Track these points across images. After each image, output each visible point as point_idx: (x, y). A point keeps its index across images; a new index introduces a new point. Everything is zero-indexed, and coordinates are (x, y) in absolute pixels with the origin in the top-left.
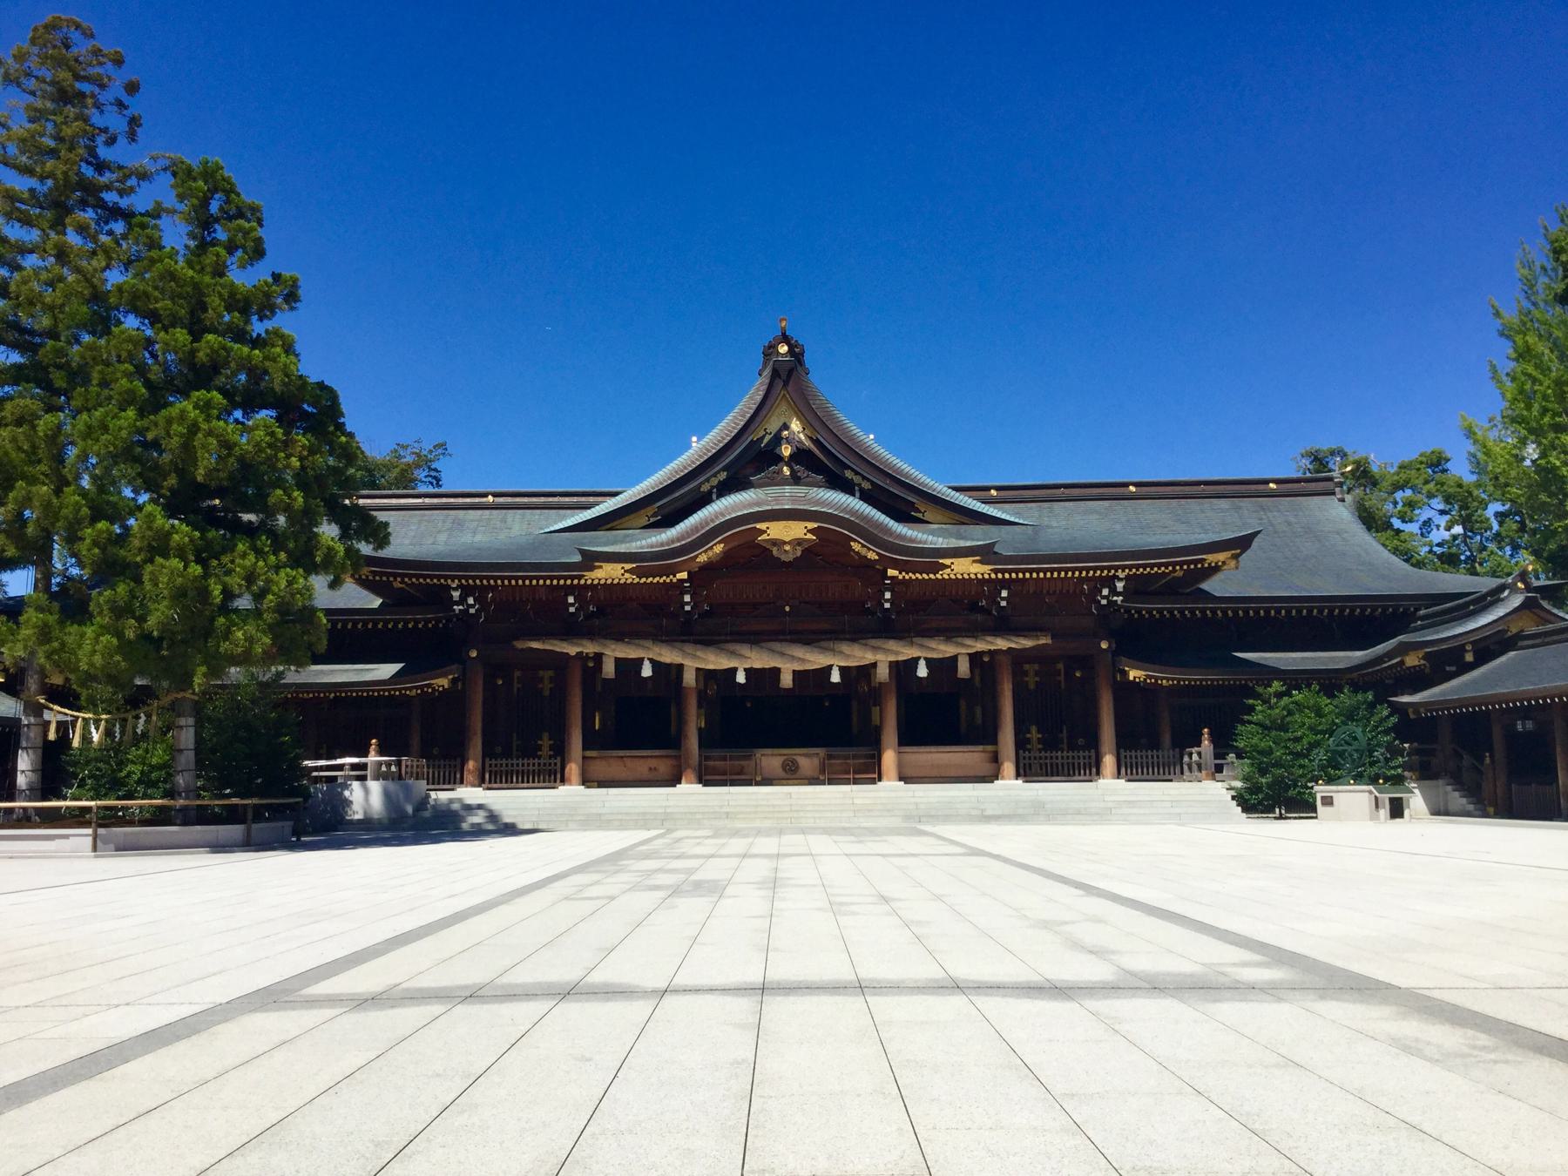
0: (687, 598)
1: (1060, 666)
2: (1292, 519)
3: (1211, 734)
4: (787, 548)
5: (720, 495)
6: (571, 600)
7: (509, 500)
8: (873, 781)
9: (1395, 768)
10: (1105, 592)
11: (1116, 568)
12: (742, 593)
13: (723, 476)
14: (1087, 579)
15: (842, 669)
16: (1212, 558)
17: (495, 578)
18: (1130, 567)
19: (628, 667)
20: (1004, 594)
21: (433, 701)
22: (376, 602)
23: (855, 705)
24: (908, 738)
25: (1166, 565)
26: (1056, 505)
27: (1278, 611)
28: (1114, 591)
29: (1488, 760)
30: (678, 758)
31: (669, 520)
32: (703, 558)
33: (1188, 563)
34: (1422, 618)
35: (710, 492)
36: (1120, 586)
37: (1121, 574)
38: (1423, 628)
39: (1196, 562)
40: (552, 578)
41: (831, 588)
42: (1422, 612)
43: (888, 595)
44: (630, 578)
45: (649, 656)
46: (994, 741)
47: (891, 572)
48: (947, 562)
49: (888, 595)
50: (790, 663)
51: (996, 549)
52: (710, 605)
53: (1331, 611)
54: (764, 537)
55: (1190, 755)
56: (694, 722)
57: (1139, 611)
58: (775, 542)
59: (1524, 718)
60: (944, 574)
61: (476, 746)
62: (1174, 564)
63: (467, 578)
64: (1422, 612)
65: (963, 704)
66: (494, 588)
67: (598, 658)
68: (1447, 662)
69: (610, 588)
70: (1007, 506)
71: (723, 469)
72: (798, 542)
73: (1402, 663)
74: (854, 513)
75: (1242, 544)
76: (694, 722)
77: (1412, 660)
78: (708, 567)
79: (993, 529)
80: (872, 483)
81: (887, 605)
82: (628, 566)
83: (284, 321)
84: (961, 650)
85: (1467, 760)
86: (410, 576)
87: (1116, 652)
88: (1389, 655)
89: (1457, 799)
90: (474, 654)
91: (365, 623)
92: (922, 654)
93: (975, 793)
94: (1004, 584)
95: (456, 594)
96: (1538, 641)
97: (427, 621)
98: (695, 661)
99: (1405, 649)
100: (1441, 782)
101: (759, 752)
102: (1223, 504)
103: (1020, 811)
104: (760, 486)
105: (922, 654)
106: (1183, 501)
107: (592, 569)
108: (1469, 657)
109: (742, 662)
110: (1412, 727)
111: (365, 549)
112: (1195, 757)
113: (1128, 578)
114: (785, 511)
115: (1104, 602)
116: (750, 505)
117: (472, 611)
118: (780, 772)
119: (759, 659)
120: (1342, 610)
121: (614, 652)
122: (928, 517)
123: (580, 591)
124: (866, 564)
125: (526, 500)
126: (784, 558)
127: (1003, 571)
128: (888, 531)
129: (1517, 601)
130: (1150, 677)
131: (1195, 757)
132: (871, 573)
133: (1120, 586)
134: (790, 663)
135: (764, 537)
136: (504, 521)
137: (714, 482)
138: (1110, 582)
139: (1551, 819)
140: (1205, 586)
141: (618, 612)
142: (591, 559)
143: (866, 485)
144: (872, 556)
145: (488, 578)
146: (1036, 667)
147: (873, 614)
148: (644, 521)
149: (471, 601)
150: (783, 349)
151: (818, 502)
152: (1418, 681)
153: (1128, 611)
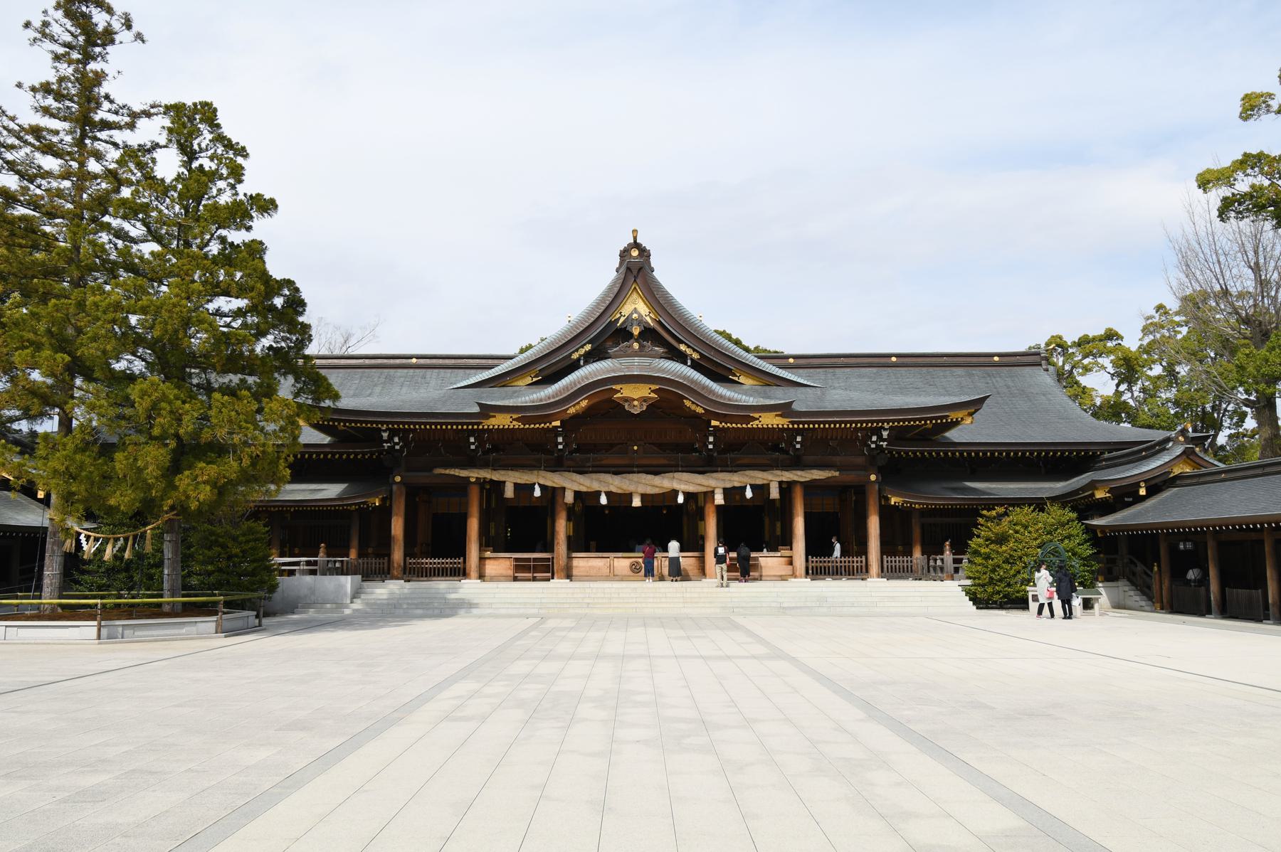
0: (560, 439)
2: (1010, 384)
4: (636, 403)
5: (586, 363)
6: (472, 440)
7: (428, 361)
9: (159, 538)
10: (874, 438)
11: (883, 422)
12: (600, 431)
13: (588, 347)
15: (725, 490)
16: (954, 415)
17: (415, 424)
18: (893, 421)
19: (527, 489)
20: (799, 439)
21: (365, 513)
22: (326, 439)
23: (685, 519)
24: (491, 542)
25: (920, 420)
26: (837, 370)
27: (1000, 453)
28: (880, 438)
29: (1156, 568)
31: (550, 378)
32: (572, 411)
33: (936, 418)
34: (1106, 460)
35: (579, 360)
36: (885, 434)
38: (1108, 467)
39: (941, 418)
40: (457, 424)
41: (674, 431)
42: (1106, 455)
43: (711, 439)
44: (517, 425)
45: (540, 480)
46: (702, 549)
47: (714, 423)
48: (756, 415)
49: (711, 439)
52: (578, 445)
53: (1039, 454)
54: (619, 395)
55: (935, 560)
56: (562, 527)
57: (899, 452)
58: (626, 400)
59: (1185, 541)
60: (755, 424)
61: (355, 542)
62: (926, 419)
63: (393, 423)
64: (1106, 455)
67: (501, 484)
68: (1125, 496)
69: (502, 431)
70: (801, 371)
71: (588, 342)
72: (644, 399)
73: (1093, 495)
74: (685, 378)
76: (562, 527)
77: (1100, 494)
78: (575, 417)
80: (701, 354)
81: (711, 447)
82: (515, 416)
83: (261, 228)
84: (773, 480)
85: (1140, 568)
86: (351, 422)
88: (1083, 489)
89: (1135, 598)
90: (398, 479)
91: (318, 454)
92: (746, 480)
94: (798, 432)
95: (385, 435)
96: (1194, 481)
97: (364, 454)
98: (572, 484)
99: (1093, 485)
100: (1120, 583)
102: (959, 371)
103: (809, 604)
104: (616, 357)
105: (746, 480)
106: (931, 369)
107: (488, 417)
108: (1142, 492)
109: (605, 485)
110: (1104, 543)
111: (328, 403)
112: (939, 563)
114: (635, 375)
115: (873, 446)
117: (397, 447)
118: (627, 572)
119: (617, 484)
120: (1047, 453)
121: (511, 480)
122: (742, 380)
123: (479, 434)
124: (696, 416)
125: (441, 361)
126: (636, 411)
127: (798, 423)
128: (711, 391)
129: (1179, 450)
131: (939, 563)
132: (700, 422)
133: (885, 434)
135: (619, 395)
136: (424, 377)
137: (582, 351)
138: (878, 431)
139: (1202, 615)
140: (947, 434)
141: (530, 444)
142: (487, 411)
143: (696, 356)
144: (700, 410)
145: (409, 424)
147: (700, 452)
148: (529, 380)
149: (396, 440)
150: (635, 253)
151: (660, 370)
153: (890, 452)
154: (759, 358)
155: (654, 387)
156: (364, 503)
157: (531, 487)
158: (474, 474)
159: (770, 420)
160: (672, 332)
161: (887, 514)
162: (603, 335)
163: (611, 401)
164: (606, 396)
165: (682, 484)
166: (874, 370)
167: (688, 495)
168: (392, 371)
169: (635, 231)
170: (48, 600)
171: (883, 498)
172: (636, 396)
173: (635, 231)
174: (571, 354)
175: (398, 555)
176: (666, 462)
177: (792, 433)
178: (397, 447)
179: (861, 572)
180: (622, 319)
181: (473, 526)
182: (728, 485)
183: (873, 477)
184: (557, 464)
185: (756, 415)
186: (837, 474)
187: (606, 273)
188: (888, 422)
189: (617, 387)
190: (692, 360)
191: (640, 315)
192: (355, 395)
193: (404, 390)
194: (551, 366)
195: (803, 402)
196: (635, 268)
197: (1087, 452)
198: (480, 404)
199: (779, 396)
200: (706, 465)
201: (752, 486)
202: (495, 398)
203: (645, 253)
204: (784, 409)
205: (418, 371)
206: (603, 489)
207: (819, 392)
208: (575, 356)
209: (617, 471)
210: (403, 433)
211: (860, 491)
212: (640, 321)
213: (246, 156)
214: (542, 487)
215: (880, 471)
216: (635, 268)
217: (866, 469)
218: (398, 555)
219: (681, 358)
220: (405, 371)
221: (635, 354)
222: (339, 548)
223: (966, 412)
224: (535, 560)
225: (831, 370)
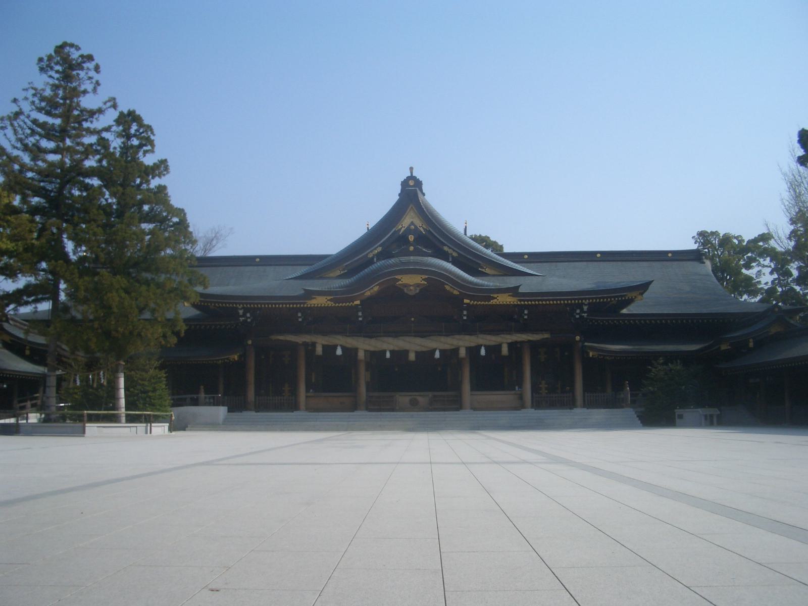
0: (360, 314)
4: (412, 288)
5: (378, 260)
6: (300, 315)
10: (578, 311)
12: (390, 310)
13: (380, 249)
16: (630, 295)
26: (558, 264)
28: (582, 311)
32: (368, 294)
35: (373, 258)
36: (585, 308)
39: (622, 296)
41: (442, 308)
43: (465, 313)
44: (330, 304)
45: (341, 343)
47: (466, 301)
48: (495, 296)
49: (465, 313)
50: (413, 345)
54: (400, 282)
56: (364, 377)
58: (406, 286)
61: (221, 388)
62: (611, 297)
63: (247, 304)
67: (314, 345)
72: (418, 285)
73: (720, 348)
78: (370, 298)
82: (329, 298)
84: (504, 341)
90: (250, 342)
92: (484, 340)
94: (526, 307)
95: (241, 312)
98: (363, 346)
101: (60, 299)
107: (311, 299)
115: (577, 316)
119: (400, 343)
121: (321, 342)
123: (304, 310)
126: (410, 293)
130: (601, 355)
133: (585, 308)
134: (413, 345)
135: (400, 282)
138: (580, 306)
142: (309, 294)
143: (455, 254)
144: (456, 292)
148: (338, 273)
149: (248, 315)
154: (497, 254)
156: (227, 359)
157: (334, 347)
160: (436, 238)
161: (589, 364)
167: (442, 352)
169: (411, 169)
170: (348, 334)
173: (411, 169)
177: (522, 307)
180: (403, 230)
185: (495, 296)
186: (546, 336)
187: (390, 198)
190: (453, 257)
191: (416, 227)
192: (219, 286)
195: (526, 286)
196: (411, 191)
199: (511, 282)
202: (315, 285)
203: (418, 184)
204: (514, 291)
206: (505, 341)
207: (540, 279)
208: (370, 256)
209: (396, 334)
212: (416, 231)
213: (154, 135)
214: (343, 348)
216: (411, 191)
219: (445, 257)
222: (211, 390)
225: (554, 264)
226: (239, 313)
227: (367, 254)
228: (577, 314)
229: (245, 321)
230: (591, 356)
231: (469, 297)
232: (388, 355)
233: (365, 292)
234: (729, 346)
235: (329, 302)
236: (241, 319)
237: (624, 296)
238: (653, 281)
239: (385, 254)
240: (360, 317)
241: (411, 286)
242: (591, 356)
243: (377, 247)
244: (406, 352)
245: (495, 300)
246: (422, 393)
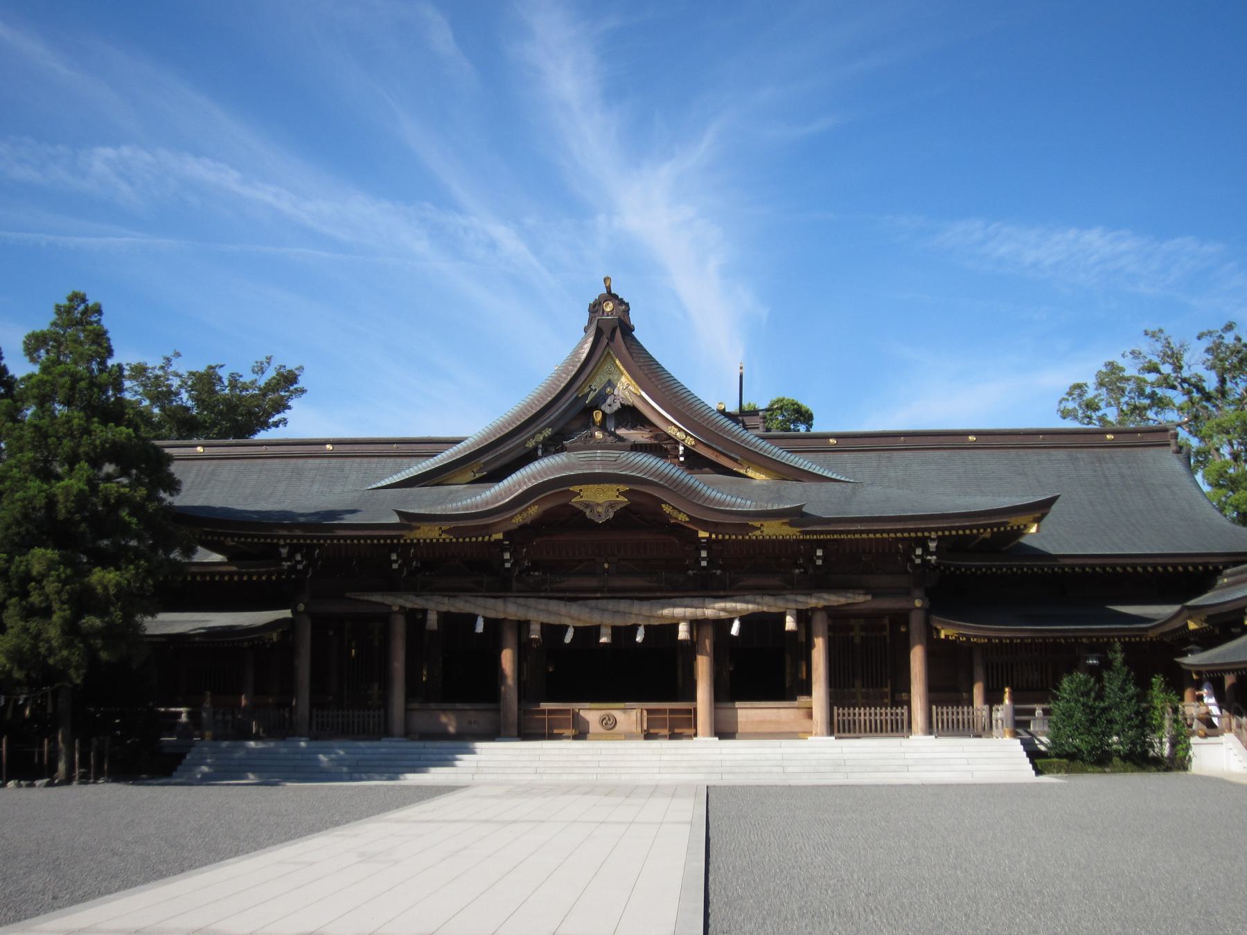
0: (507, 556)
1: (886, 621)
3: (1011, 694)
4: (600, 509)
5: (547, 453)
6: (394, 557)
8: (690, 737)
10: (919, 552)
11: (930, 530)
12: (554, 543)
13: (548, 432)
14: (903, 539)
16: (1015, 521)
18: (943, 529)
20: (819, 553)
26: (895, 454)
28: (926, 551)
30: (498, 710)
31: (496, 476)
32: (518, 520)
35: (536, 449)
37: (933, 535)
39: (999, 525)
41: (653, 543)
43: (704, 554)
45: (483, 610)
47: (703, 534)
49: (704, 554)
51: (804, 510)
58: (587, 505)
65: (788, 658)
66: (320, 546)
69: (431, 545)
71: (548, 426)
72: (612, 505)
75: (1040, 509)
78: (523, 527)
79: (813, 486)
87: (928, 612)
92: (731, 610)
93: (779, 751)
95: (284, 551)
101: (738, 704)
102: (1061, 454)
106: (1022, 452)
107: (411, 528)
109: (572, 617)
113: (939, 539)
115: (918, 561)
116: (566, 467)
117: (300, 567)
121: (435, 607)
122: (750, 473)
123: (403, 549)
124: (679, 527)
130: (963, 635)
138: (922, 542)
141: (467, 558)
142: (410, 520)
146: (862, 621)
148: (470, 476)
149: (298, 557)
151: (629, 466)
152: (1207, 640)
155: (623, 488)
158: (397, 602)
159: (773, 530)
161: (938, 655)
162: (568, 414)
163: (567, 506)
164: (561, 501)
165: (642, 616)
166: (945, 453)
168: (301, 461)
171: (930, 631)
172: (602, 500)
174: (525, 442)
175: (302, 702)
176: (647, 584)
178: (300, 567)
179: (901, 728)
181: (859, 599)
182: (801, 607)
183: (918, 603)
184: (501, 585)
185: (757, 524)
188: (936, 530)
189: (576, 488)
193: (316, 487)
194: (495, 458)
196: (612, 330)
197: (1205, 565)
198: (400, 514)
199: (793, 495)
200: (707, 588)
201: (646, 627)
204: (796, 516)
205: (334, 461)
208: (531, 444)
210: (307, 550)
211: (902, 617)
215: (929, 594)
217: (907, 593)
218: (302, 702)
220: (318, 461)
221: (601, 446)
223: (1031, 517)
224: (672, 711)
225: (887, 454)
226: (280, 554)
227: (525, 442)
228: (918, 557)
229: (292, 569)
230: (943, 636)
231: (705, 525)
232: (480, 628)
233: (512, 517)
234: (1206, 621)
235: (444, 536)
236: (286, 564)
237: (1005, 524)
238: (1049, 503)
239: (554, 445)
240: (507, 561)
241: (598, 505)
242: (943, 636)
243: (543, 428)
244: (595, 631)
245: (758, 533)
246: (621, 705)
